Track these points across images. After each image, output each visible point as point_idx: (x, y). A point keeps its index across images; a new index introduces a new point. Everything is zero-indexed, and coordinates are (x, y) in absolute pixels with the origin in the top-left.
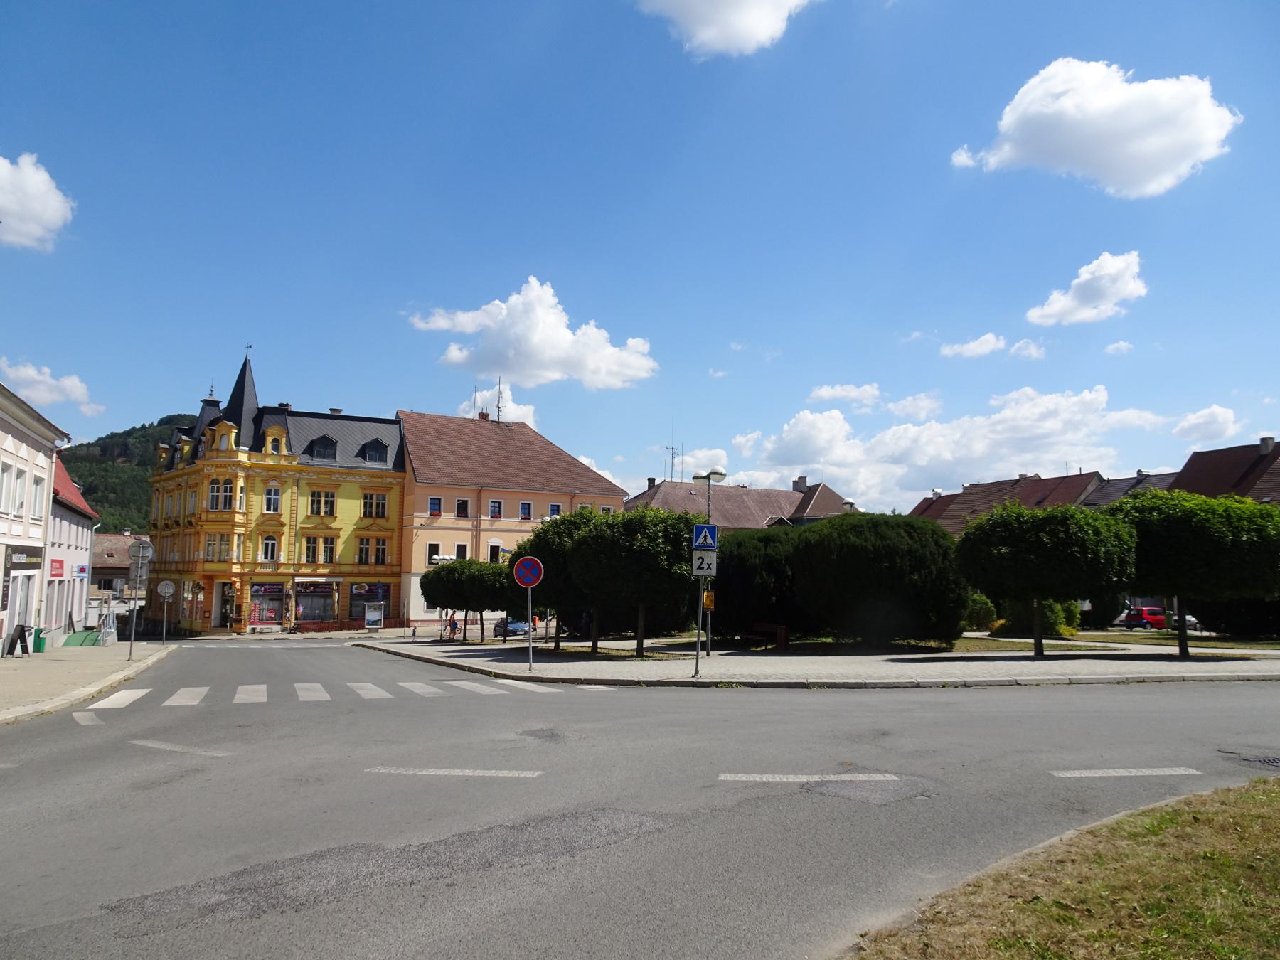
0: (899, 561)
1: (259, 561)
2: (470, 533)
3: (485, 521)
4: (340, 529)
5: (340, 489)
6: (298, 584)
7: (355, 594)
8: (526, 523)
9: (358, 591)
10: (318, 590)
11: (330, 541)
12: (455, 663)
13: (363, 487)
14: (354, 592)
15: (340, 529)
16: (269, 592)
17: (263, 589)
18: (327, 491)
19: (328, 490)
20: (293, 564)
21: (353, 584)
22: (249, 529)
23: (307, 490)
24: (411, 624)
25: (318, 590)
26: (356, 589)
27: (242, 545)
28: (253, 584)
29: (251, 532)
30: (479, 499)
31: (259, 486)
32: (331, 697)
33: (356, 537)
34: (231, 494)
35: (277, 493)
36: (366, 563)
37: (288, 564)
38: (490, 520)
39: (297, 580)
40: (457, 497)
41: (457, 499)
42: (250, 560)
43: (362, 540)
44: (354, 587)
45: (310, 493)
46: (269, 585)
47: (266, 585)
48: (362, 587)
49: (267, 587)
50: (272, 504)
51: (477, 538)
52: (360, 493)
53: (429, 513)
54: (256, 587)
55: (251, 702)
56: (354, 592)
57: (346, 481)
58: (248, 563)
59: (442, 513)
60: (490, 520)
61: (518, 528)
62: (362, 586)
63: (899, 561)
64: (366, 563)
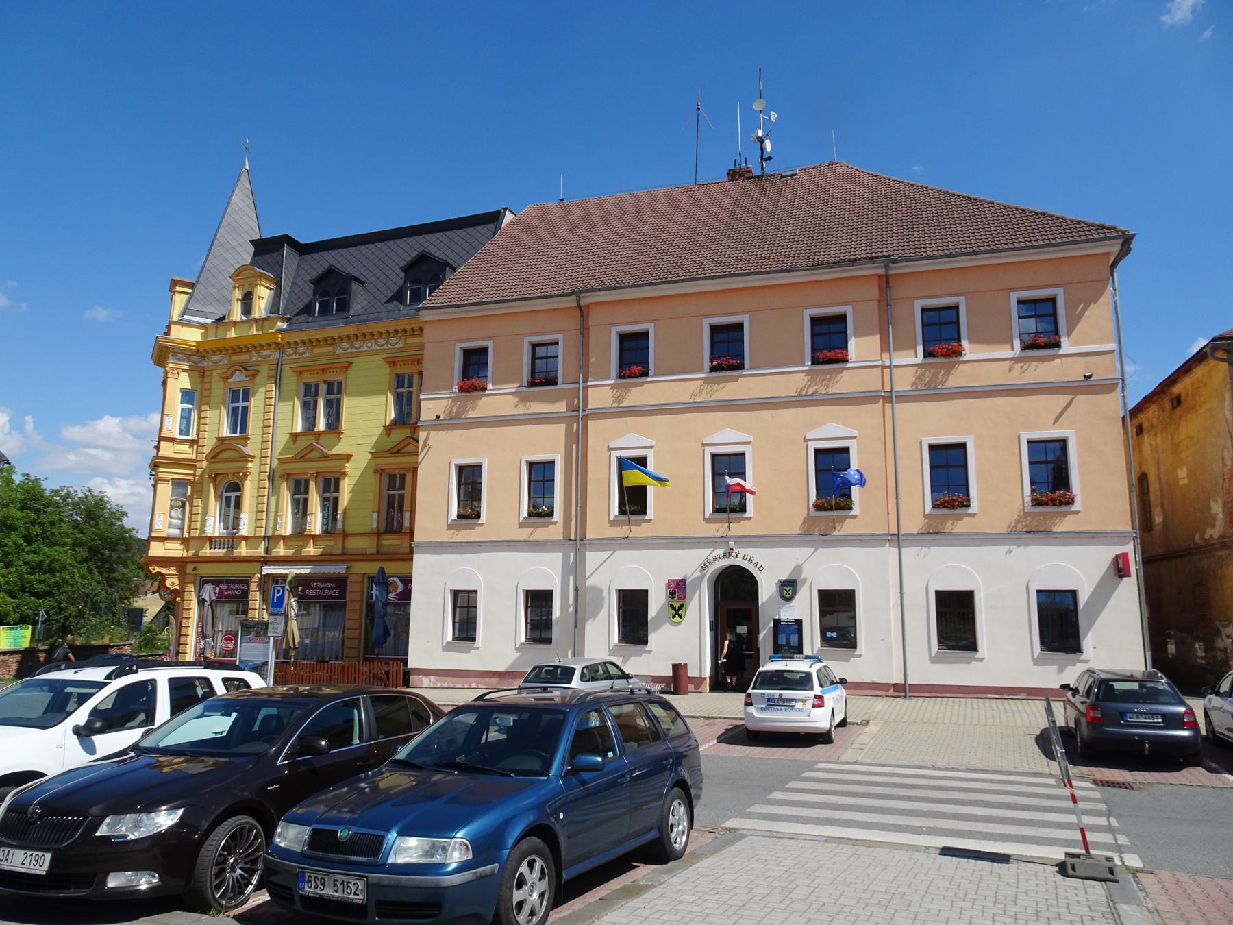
0: (58, 499)
1: (209, 532)
2: (561, 428)
3: (601, 394)
4: (348, 457)
5: (351, 372)
8: (636, 385)
10: (309, 592)
11: (331, 485)
12: (936, 810)
13: (392, 363)
15: (348, 457)
16: (227, 597)
18: (308, 381)
19: (330, 377)
20: (264, 538)
22: (199, 472)
23: (291, 380)
24: (413, 678)
25: (309, 592)
27: (187, 504)
28: (204, 581)
29: (202, 476)
30: (584, 331)
31: (218, 388)
32: (1143, 863)
33: (380, 471)
34: (245, 404)
35: (246, 398)
37: (255, 537)
38: (807, 373)
39: (268, 570)
40: (707, 316)
41: (1014, 296)
42: (197, 533)
43: (392, 478)
45: (302, 389)
46: (228, 581)
47: (222, 582)
49: (223, 586)
50: (240, 419)
51: (577, 440)
52: (385, 374)
53: (920, 349)
55: (1023, 845)
57: (360, 354)
58: (194, 538)
59: (965, 343)
60: (613, 386)
61: (521, 410)
63: (58, 499)
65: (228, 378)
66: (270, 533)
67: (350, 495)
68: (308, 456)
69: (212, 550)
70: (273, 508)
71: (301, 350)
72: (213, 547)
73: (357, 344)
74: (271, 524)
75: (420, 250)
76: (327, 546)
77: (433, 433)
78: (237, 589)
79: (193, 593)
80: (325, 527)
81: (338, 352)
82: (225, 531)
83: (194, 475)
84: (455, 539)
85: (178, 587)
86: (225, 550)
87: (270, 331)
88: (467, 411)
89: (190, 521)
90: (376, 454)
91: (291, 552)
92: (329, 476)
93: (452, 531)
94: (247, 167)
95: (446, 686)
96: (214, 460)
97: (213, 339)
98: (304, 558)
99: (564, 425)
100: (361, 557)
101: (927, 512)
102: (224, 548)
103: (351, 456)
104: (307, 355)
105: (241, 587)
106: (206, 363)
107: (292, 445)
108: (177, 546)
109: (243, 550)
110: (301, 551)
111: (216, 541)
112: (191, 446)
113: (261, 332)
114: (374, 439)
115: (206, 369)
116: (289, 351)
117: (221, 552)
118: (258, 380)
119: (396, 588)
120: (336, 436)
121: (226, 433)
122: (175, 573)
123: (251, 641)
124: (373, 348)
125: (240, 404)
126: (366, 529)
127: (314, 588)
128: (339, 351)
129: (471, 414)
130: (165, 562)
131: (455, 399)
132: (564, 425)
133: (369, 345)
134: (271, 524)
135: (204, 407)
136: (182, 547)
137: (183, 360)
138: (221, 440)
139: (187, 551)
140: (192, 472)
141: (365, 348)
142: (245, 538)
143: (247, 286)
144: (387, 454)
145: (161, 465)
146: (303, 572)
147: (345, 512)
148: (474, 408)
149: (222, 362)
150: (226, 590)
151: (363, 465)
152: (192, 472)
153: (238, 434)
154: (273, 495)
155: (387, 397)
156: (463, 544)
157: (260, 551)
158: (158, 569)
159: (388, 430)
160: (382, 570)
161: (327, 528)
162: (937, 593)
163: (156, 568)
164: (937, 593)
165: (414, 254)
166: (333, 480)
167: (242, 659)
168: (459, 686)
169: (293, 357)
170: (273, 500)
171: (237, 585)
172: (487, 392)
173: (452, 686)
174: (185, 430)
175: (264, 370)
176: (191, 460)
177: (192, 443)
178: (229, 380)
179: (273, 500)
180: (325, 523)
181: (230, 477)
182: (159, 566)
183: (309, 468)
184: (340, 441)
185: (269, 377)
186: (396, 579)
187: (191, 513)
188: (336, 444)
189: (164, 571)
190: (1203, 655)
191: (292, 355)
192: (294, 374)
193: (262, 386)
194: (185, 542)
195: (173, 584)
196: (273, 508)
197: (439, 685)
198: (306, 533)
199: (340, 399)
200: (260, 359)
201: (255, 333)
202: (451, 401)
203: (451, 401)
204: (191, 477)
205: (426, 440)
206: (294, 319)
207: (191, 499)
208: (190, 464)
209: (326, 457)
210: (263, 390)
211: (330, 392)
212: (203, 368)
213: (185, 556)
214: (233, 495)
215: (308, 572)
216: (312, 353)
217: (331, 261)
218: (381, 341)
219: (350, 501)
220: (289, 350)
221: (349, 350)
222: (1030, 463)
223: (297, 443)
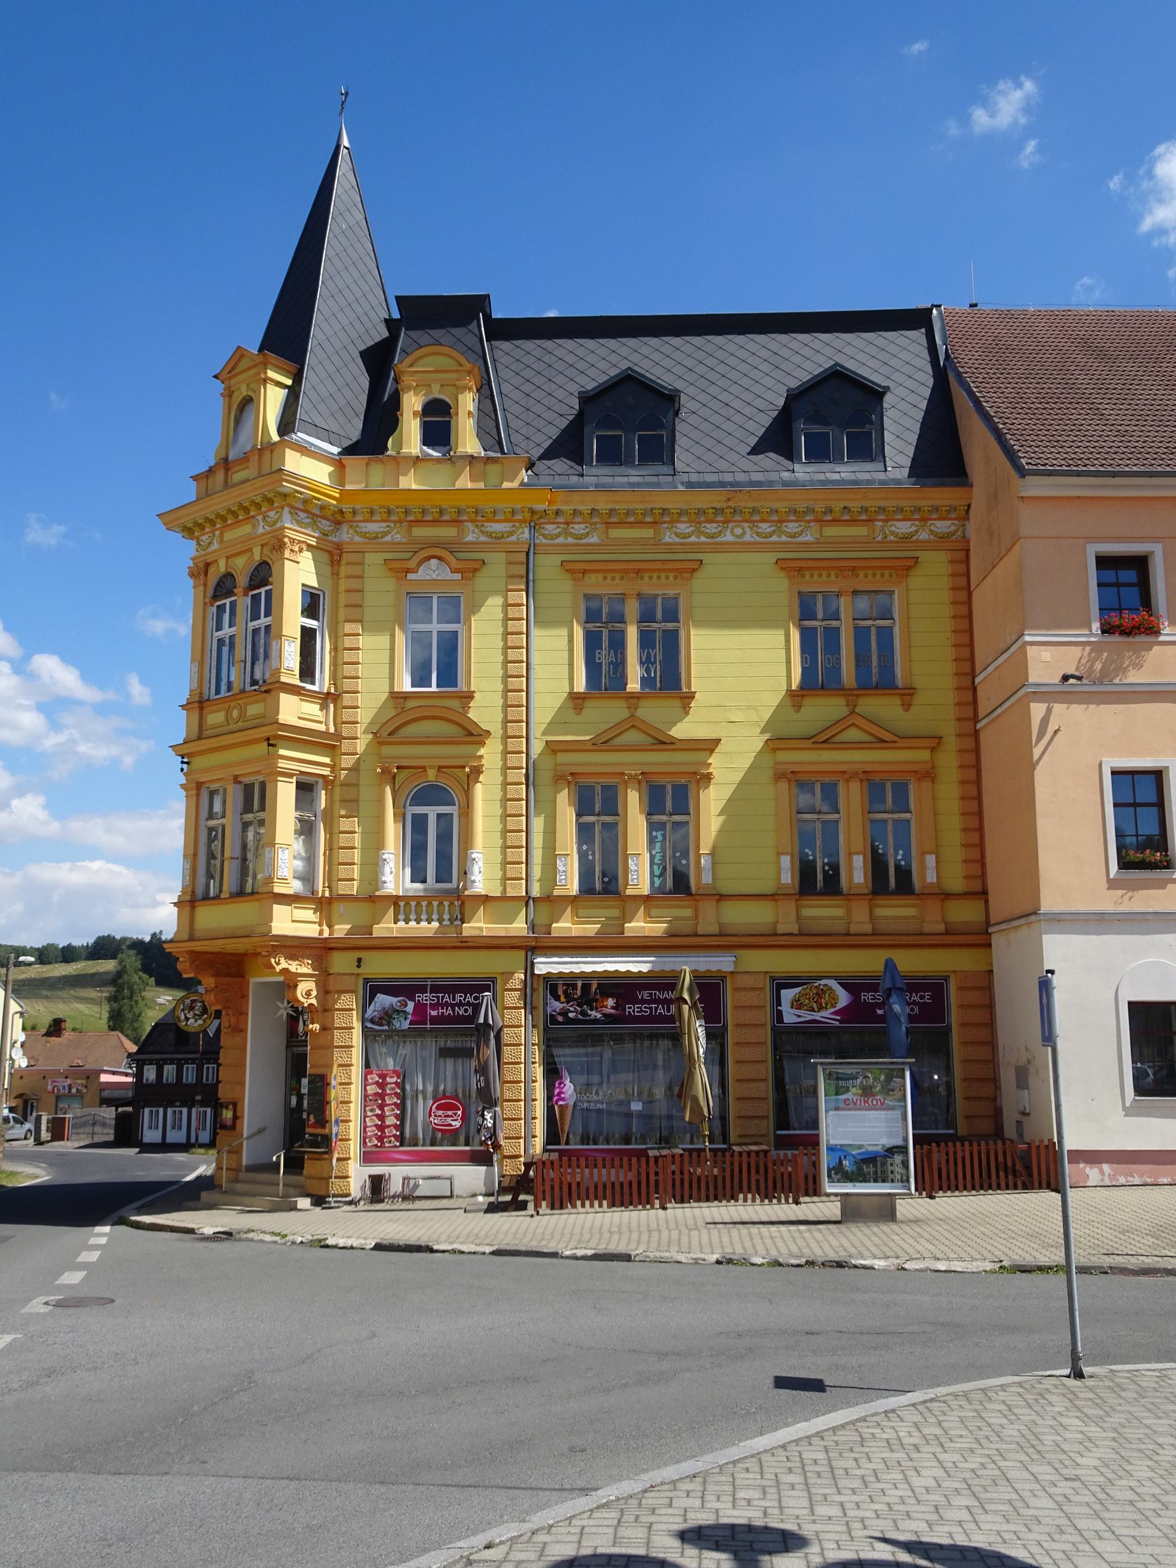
4: (711, 745)
5: (699, 582)
6: (552, 984)
7: (798, 1030)
9: (808, 1016)
10: (631, 1009)
14: (790, 1017)
15: (711, 745)
16: (434, 1020)
17: (410, 1006)
21: (780, 983)
22: (347, 761)
25: (631, 1009)
26: (797, 1004)
28: (373, 988)
29: (355, 769)
36: (832, 886)
37: (503, 898)
39: (545, 965)
44: (787, 995)
46: (435, 989)
47: (422, 989)
48: (820, 998)
49: (426, 998)
54: (384, 1001)
56: (790, 1017)
62: (820, 993)
64: (832, 886)
65: (408, 571)
66: (536, 891)
67: (722, 818)
68: (617, 741)
69: (401, 924)
70: (538, 841)
71: (579, 528)
72: (401, 917)
73: (712, 528)
74: (537, 872)
75: (624, 365)
76: (676, 919)
77: (1058, 708)
78: (460, 1005)
79: (354, 1013)
80: (657, 882)
81: (667, 539)
82: (418, 885)
83: (332, 767)
84: (1125, 907)
85: (314, 1001)
86: (435, 924)
87: (506, 485)
88: (1125, 670)
89: (330, 861)
90: (777, 742)
91: (591, 929)
92: (661, 780)
93: (1121, 892)
94: (347, 145)
95: (1137, 1181)
96: (391, 739)
97: (361, 486)
98: (376, 943)
99: (1032, 705)
100: (760, 940)
101: (1112, 876)
102: (429, 921)
103: (718, 741)
104: (594, 539)
105: (917, 999)
106: (345, 535)
107: (571, 715)
108: (308, 914)
109: (479, 925)
110: (371, 927)
111: (407, 904)
112: (324, 707)
113: (481, 485)
114: (767, 714)
115: (346, 548)
116: (550, 528)
117: (427, 928)
118: (481, 581)
119: (834, 999)
120: (677, 703)
121: (405, 684)
122: (310, 971)
123: (849, 1106)
124: (747, 538)
125: (263, 621)
126: (768, 887)
127: (643, 1002)
128: (668, 537)
129: (1134, 677)
130: (296, 947)
131: (1096, 648)
132: (1032, 705)
133: (738, 531)
134: (537, 872)
135: (349, 628)
136: (314, 917)
137: (306, 526)
138: (397, 698)
139: (330, 926)
140: (327, 760)
141: (728, 537)
142: (486, 899)
143: (436, 388)
144: (808, 744)
145: (280, 742)
146: (634, 968)
147: (712, 854)
148: (1138, 666)
149: (388, 538)
150: (433, 1007)
151: (746, 762)
152: (327, 760)
153: (434, 688)
154: (537, 815)
155: (393, 636)
156: (1149, 917)
157: (519, 926)
158: (284, 964)
159: (795, 698)
160: (890, 964)
161: (663, 883)
162: (1132, 1005)
163: (282, 960)
164: (1132, 1005)
165: (613, 372)
166: (669, 788)
167: (832, 1142)
168: (1165, 1181)
169: (560, 540)
170: (538, 823)
171: (459, 997)
172: (1162, 638)
173: (1149, 1180)
174: (307, 671)
175: (497, 563)
176: (325, 734)
177: (326, 699)
178: (411, 576)
179: (538, 823)
180: (658, 869)
181: (432, 774)
182: (291, 957)
183: (624, 764)
184: (687, 713)
185: (511, 577)
186: (833, 984)
187: (330, 848)
188: (681, 720)
189: (294, 967)
190: (370, 1092)
191: (557, 536)
192: (783, 574)
193: (494, 593)
194: (324, 906)
195: (308, 994)
196: (538, 841)
197: (1122, 1180)
198: (629, 892)
199: (675, 633)
200: (483, 538)
201: (469, 485)
202: (1088, 649)
203: (1088, 649)
204: (326, 772)
205: (1045, 721)
206: (538, 464)
207: (329, 817)
208: (327, 743)
209: (664, 743)
210: (498, 601)
211: (646, 616)
212: (339, 546)
213: (326, 934)
214: (432, 812)
215: (645, 968)
216: (221, 541)
217: (635, 358)
218: (765, 527)
219: (722, 831)
220: (549, 527)
221: (693, 539)
222: (1116, 805)
223: (584, 712)
